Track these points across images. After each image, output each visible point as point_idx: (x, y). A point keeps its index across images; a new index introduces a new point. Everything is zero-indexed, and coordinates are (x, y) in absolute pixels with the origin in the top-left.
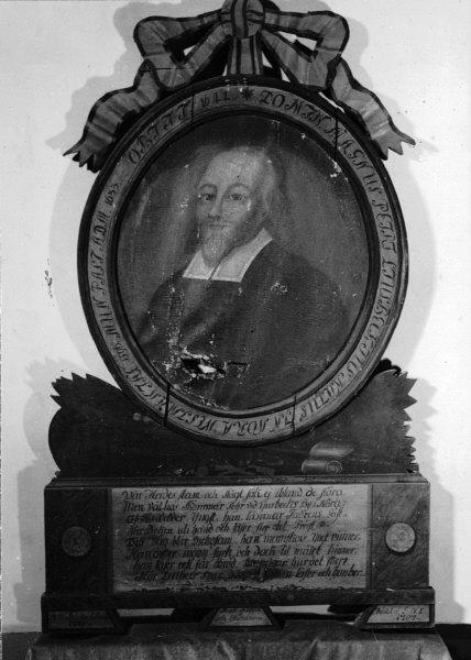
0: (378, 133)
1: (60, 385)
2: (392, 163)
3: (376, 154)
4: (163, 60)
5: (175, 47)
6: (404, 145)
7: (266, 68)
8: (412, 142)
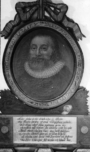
0: (77, 35)
1: (88, 92)
2: (80, 42)
3: (76, 40)
4: (21, 12)
5: (24, 9)
6: (83, 38)
7: (46, 16)
8: (84, 36)
